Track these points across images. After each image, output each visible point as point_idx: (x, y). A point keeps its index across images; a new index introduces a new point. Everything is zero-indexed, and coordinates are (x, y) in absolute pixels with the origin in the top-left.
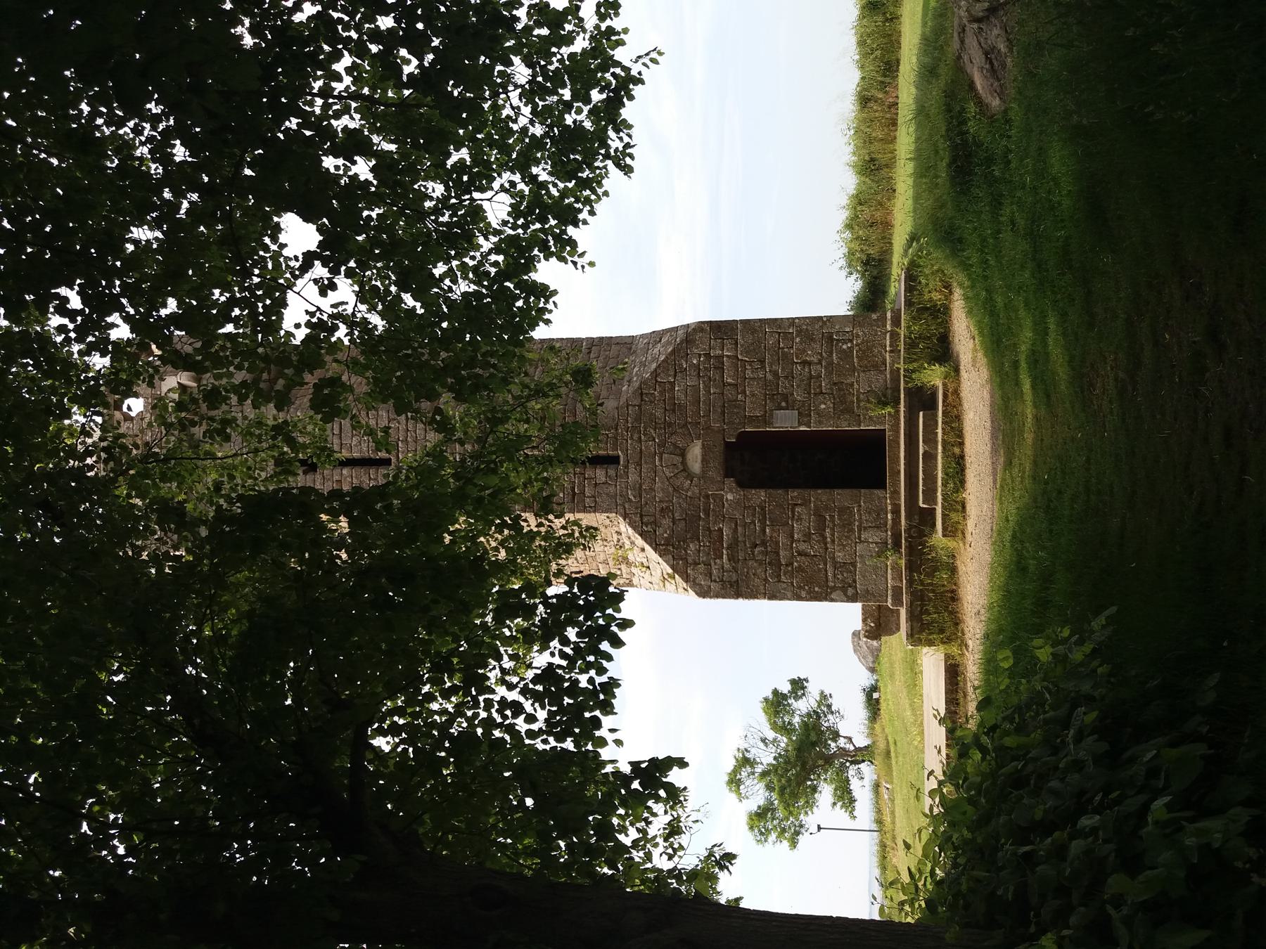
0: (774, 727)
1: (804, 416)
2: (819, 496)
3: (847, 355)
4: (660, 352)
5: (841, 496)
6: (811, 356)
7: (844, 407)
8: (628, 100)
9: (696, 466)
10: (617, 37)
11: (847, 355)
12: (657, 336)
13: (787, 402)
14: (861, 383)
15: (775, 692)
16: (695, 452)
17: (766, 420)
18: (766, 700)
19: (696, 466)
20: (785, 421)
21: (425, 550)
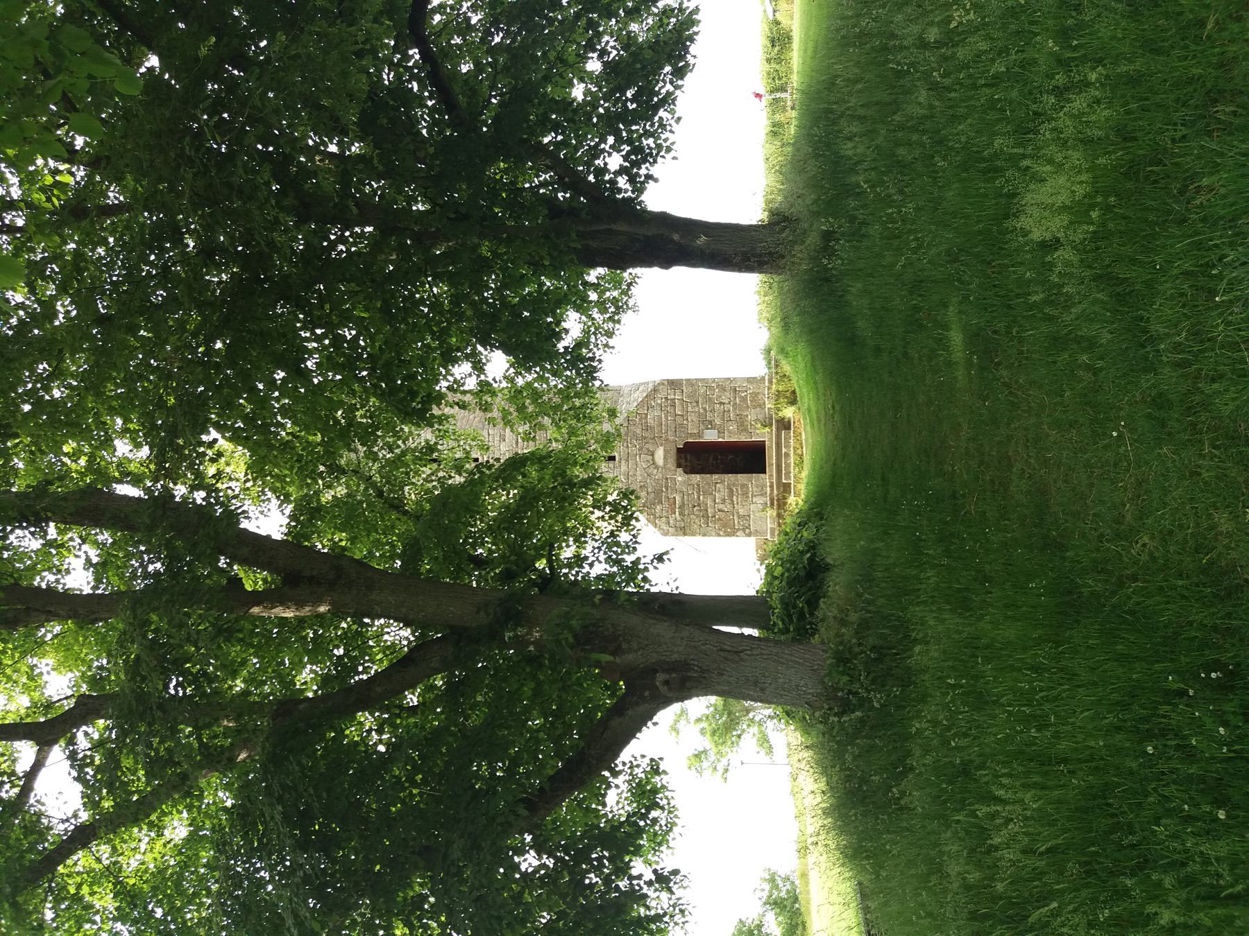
3: (744, 399)
4: (639, 396)
5: (742, 478)
7: (742, 427)
11: (744, 399)
13: (711, 425)
14: (751, 415)
16: (660, 454)
17: (700, 435)
20: (711, 436)
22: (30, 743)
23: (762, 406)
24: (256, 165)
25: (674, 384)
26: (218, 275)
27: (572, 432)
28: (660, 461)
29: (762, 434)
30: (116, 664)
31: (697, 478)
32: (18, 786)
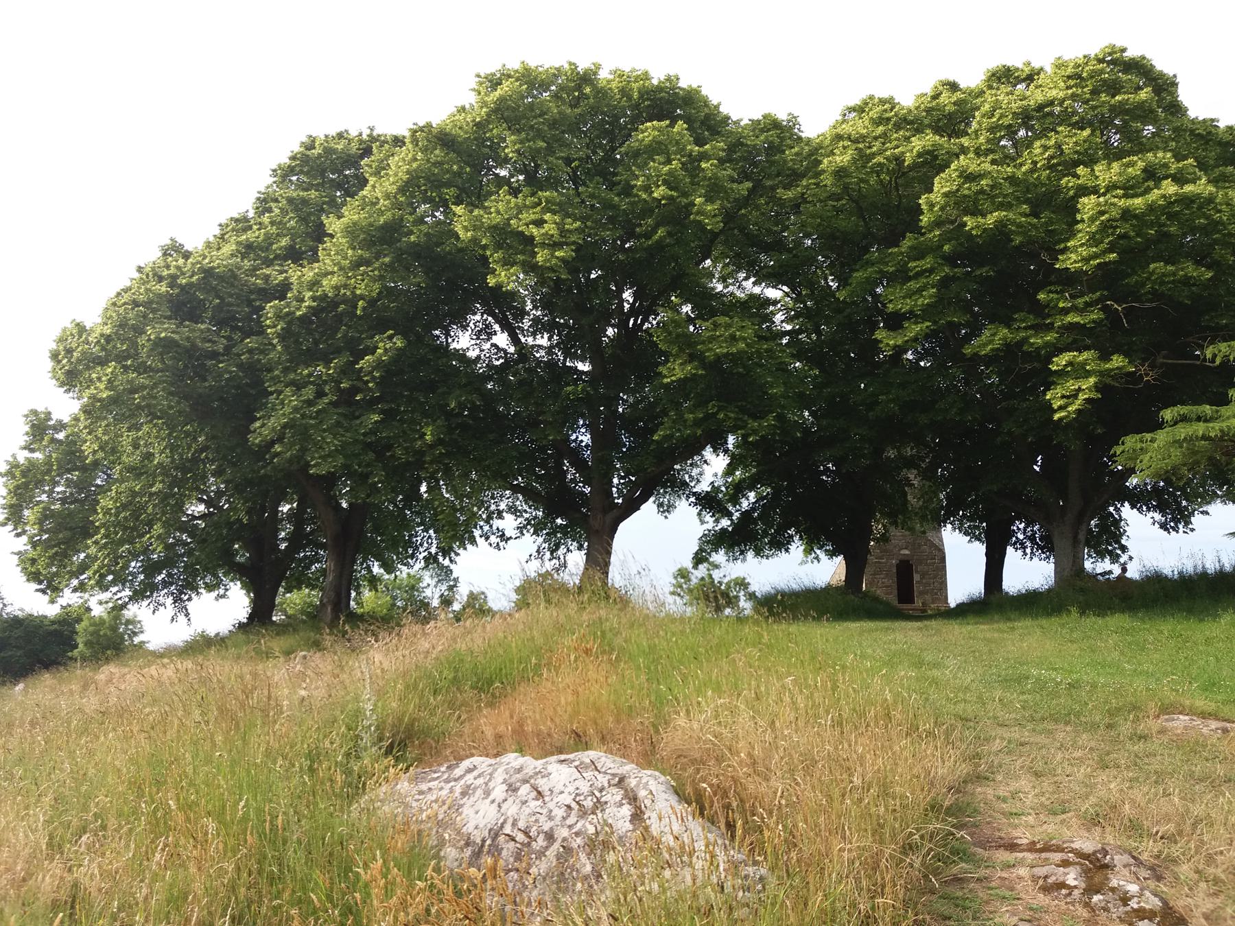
0: (730, 582)
1: (917, 582)
2: (895, 586)
3: (936, 594)
4: (936, 541)
5: (896, 592)
6: (936, 584)
7: (921, 593)
8: (50, 419)
9: (902, 552)
10: (942, 185)
11: (936, 594)
12: (941, 540)
13: (923, 576)
14: (928, 597)
15: (749, 584)
16: (907, 552)
17: (917, 572)
18: (744, 579)
19: (902, 552)
20: (916, 577)
21: (476, 212)
22: (1051, 581)
23: (933, 603)
24: (379, 482)
25: (943, 559)
26: (885, 356)
27: (916, 514)
28: (903, 552)
29: (918, 603)
30: (510, 247)
31: (895, 570)
32: (165, 363)
